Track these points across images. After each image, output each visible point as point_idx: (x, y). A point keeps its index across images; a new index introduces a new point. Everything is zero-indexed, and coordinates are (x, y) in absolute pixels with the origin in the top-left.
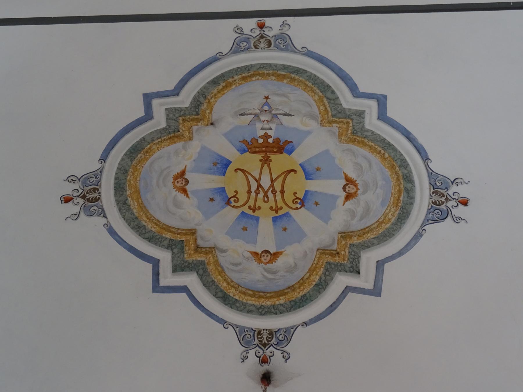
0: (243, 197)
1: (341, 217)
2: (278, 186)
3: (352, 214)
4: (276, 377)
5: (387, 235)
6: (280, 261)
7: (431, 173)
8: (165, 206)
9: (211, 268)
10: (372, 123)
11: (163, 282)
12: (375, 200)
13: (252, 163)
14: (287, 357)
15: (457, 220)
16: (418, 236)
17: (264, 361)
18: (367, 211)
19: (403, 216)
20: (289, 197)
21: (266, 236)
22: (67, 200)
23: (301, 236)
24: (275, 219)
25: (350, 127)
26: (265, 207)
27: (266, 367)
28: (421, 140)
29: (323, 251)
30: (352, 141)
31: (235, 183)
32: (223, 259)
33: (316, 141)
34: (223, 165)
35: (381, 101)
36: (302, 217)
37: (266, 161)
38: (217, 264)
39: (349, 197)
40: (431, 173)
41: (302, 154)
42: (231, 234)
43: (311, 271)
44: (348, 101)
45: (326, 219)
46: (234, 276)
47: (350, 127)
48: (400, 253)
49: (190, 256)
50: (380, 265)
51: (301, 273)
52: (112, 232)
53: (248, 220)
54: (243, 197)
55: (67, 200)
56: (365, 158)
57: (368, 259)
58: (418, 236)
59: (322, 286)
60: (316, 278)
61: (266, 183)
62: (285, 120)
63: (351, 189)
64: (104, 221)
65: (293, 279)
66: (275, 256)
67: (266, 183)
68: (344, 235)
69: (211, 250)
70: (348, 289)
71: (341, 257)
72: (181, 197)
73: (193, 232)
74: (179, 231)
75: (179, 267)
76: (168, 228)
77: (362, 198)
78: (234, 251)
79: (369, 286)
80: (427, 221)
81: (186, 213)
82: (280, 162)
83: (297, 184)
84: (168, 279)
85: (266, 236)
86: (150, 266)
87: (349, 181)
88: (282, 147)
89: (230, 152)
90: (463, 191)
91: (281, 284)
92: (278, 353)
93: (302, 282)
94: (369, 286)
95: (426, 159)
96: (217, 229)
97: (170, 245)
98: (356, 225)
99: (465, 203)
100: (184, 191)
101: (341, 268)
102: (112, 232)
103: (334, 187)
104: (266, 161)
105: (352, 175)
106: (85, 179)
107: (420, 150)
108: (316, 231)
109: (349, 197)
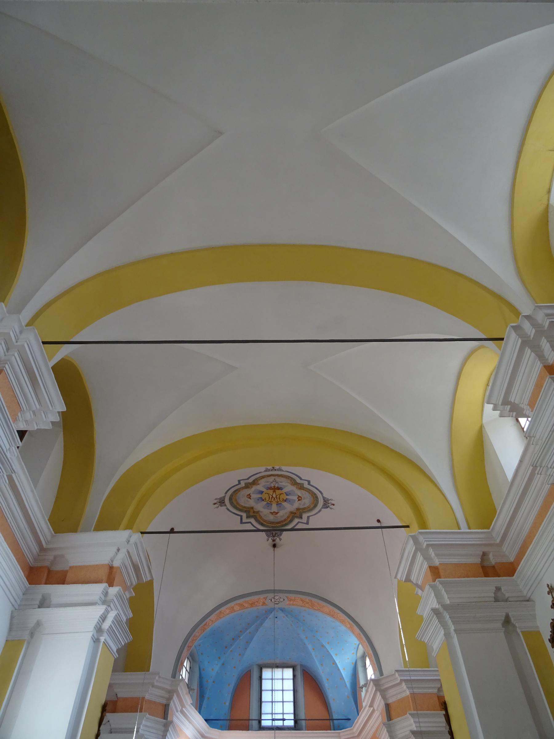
0: (267, 499)
1: (297, 505)
2: (278, 497)
3: (300, 504)
4: (277, 545)
5: (311, 510)
6: (278, 515)
7: (323, 497)
8: (243, 501)
9: (258, 517)
10: (306, 485)
11: (243, 521)
12: (307, 501)
13: (271, 492)
14: (280, 540)
15: (331, 508)
16: (320, 511)
17: (274, 541)
18: (304, 504)
19: (316, 506)
20: (281, 499)
21: (274, 508)
22: (215, 504)
23: (285, 508)
24: (277, 504)
25: (301, 487)
26: (274, 501)
27: (274, 542)
28: (321, 490)
29: (291, 513)
30: (300, 489)
31: (264, 496)
32: (261, 514)
33: (289, 488)
34: (262, 492)
35: (309, 482)
36: (285, 504)
37: (274, 491)
38: (260, 515)
39: (299, 500)
40: (323, 497)
41: (285, 490)
42: (264, 508)
43: (288, 517)
44: (298, 481)
45: (292, 505)
46: (265, 518)
47: (301, 487)
48: (315, 515)
49: (251, 514)
50: (308, 517)
51: (285, 517)
52: (228, 509)
53: (269, 505)
54: (267, 499)
55: (215, 504)
56: (349, 623)
57: (305, 516)
58: (320, 511)
59: (291, 521)
60: (289, 519)
61: (274, 496)
62: (280, 483)
63: (300, 498)
64: (225, 507)
65: (282, 519)
66: (277, 513)
67: (274, 496)
68: (298, 509)
69: (258, 512)
70: (299, 522)
71: (298, 514)
72: (249, 499)
73: (252, 508)
74: (248, 508)
75: (248, 517)
76: (245, 507)
77: (303, 501)
78: (265, 513)
79: (306, 522)
80: (322, 508)
81: (251, 503)
82: (278, 492)
83: (284, 497)
84: (245, 520)
85: (274, 508)
86: (240, 517)
87: (299, 497)
88: (279, 488)
89: (264, 490)
90: (333, 502)
91: (279, 520)
92: (278, 539)
93: (285, 520)
94: (306, 522)
95: (322, 494)
96: (260, 507)
97: (245, 512)
98: (301, 507)
99: (334, 505)
100: (250, 498)
101: (297, 517)
102: (228, 509)
103: (295, 498)
104: (274, 491)
105: (300, 495)
106: (220, 499)
107: (320, 492)
108: (289, 508)
109: (299, 500)
